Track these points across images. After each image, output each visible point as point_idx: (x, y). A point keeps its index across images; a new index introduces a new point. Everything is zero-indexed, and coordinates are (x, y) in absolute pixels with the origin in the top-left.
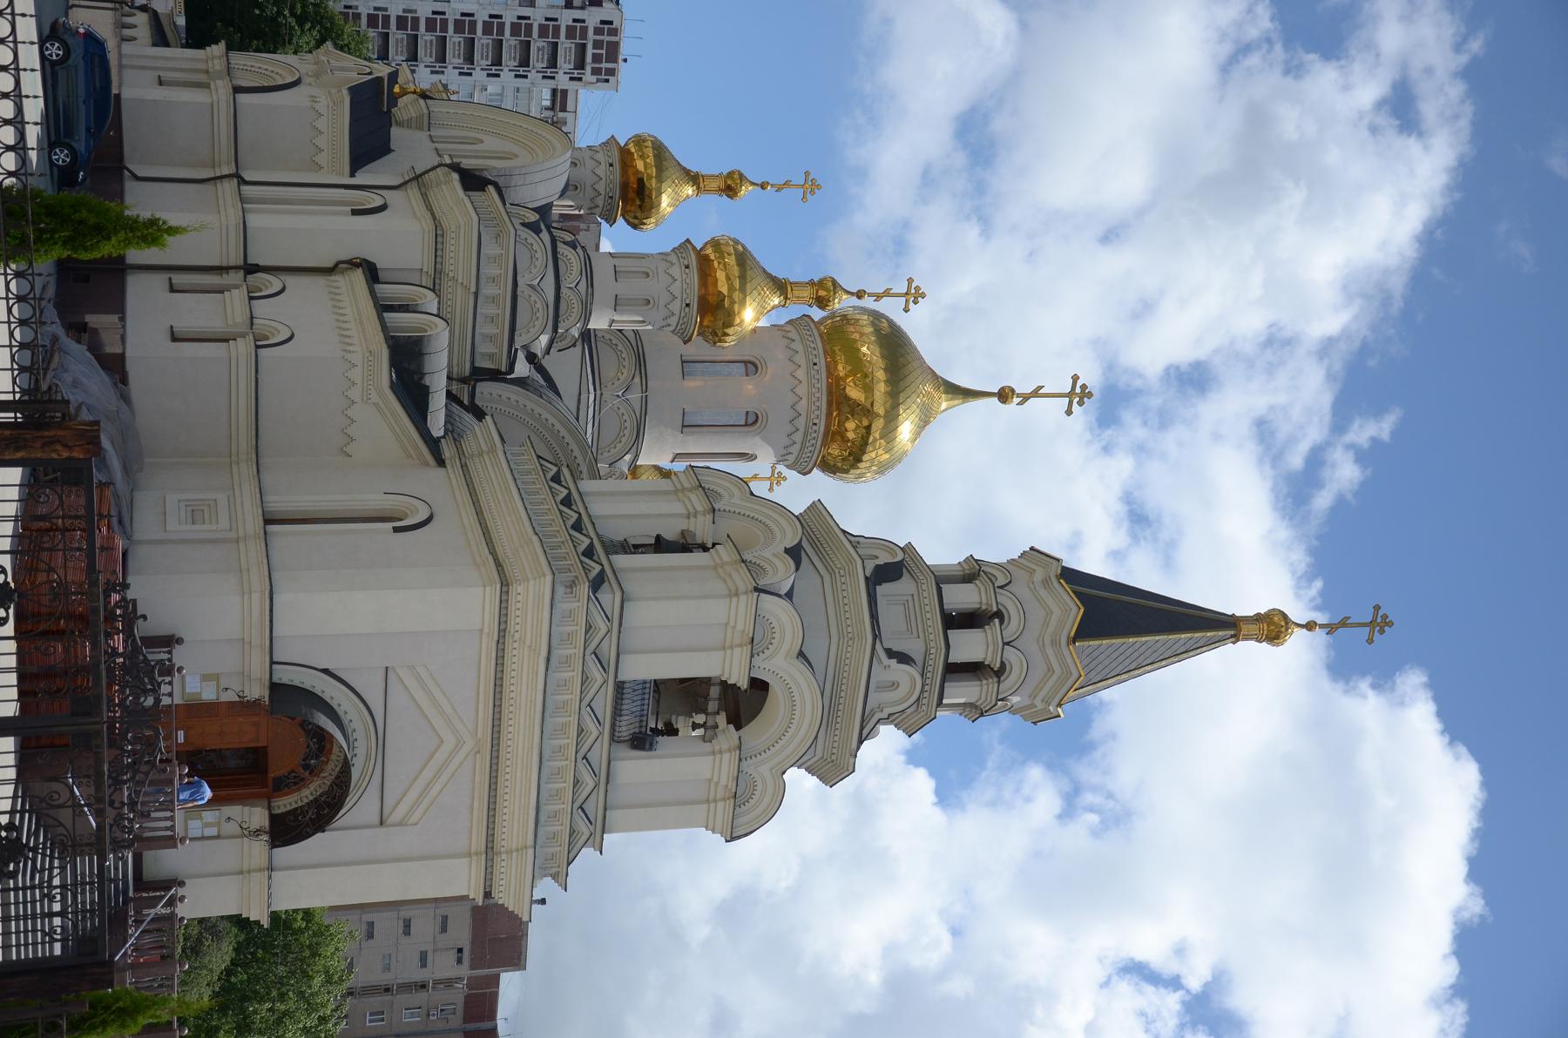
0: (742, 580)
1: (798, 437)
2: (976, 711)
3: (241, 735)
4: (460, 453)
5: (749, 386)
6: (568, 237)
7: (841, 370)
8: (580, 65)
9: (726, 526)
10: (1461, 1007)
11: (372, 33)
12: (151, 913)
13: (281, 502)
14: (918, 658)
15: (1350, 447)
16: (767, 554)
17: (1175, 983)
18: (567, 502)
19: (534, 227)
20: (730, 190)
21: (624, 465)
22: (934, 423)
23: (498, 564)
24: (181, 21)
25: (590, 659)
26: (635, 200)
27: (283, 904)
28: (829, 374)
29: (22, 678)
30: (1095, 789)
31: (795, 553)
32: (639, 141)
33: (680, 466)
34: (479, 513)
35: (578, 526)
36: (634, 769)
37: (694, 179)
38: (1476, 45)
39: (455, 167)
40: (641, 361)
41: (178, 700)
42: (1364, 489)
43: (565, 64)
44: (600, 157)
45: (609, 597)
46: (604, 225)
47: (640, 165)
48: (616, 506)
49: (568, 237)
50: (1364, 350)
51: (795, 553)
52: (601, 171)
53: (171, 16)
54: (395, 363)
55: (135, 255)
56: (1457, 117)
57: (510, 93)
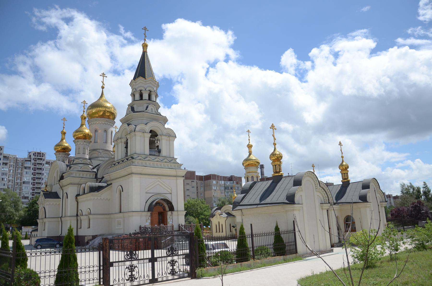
0: (133, 134)
1: (109, 123)
3: (156, 216)
4: (110, 181)
5: (99, 131)
6: (72, 162)
7: (97, 115)
8: (41, 159)
9: (123, 136)
10: (214, 27)
11: (35, 195)
12: (183, 229)
13: (118, 210)
14: (147, 105)
15: (124, 33)
16: (129, 129)
17: (208, 69)
18: (119, 163)
19: (70, 168)
20: (64, 133)
21: (113, 153)
22: (107, 100)
23: (129, 175)
24: (33, 227)
25: (145, 159)
26: (66, 150)
27: (183, 209)
28: (98, 117)
29: (146, 249)
30: (178, 79)
31: (128, 125)
32: (55, 149)
33: (113, 144)
34: (120, 178)
35: (123, 161)
36: (164, 152)
37: (62, 140)
38: (57, 7)
39: (59, 181)
41: (150, 226)
42: (132, 31)
43: (41, 162)
44: (58, 156)
45: (135, 156)
46: (70, 156)
47: (59, 149)
48: (120, 155)
49: (72, 162)
50: (108, 29)
51: (128, 125)
52: (60, 156)
53: (32, 228)
54: (94, 192)
55: (75, 233)
56: (69, 11)
57: (46, 172)
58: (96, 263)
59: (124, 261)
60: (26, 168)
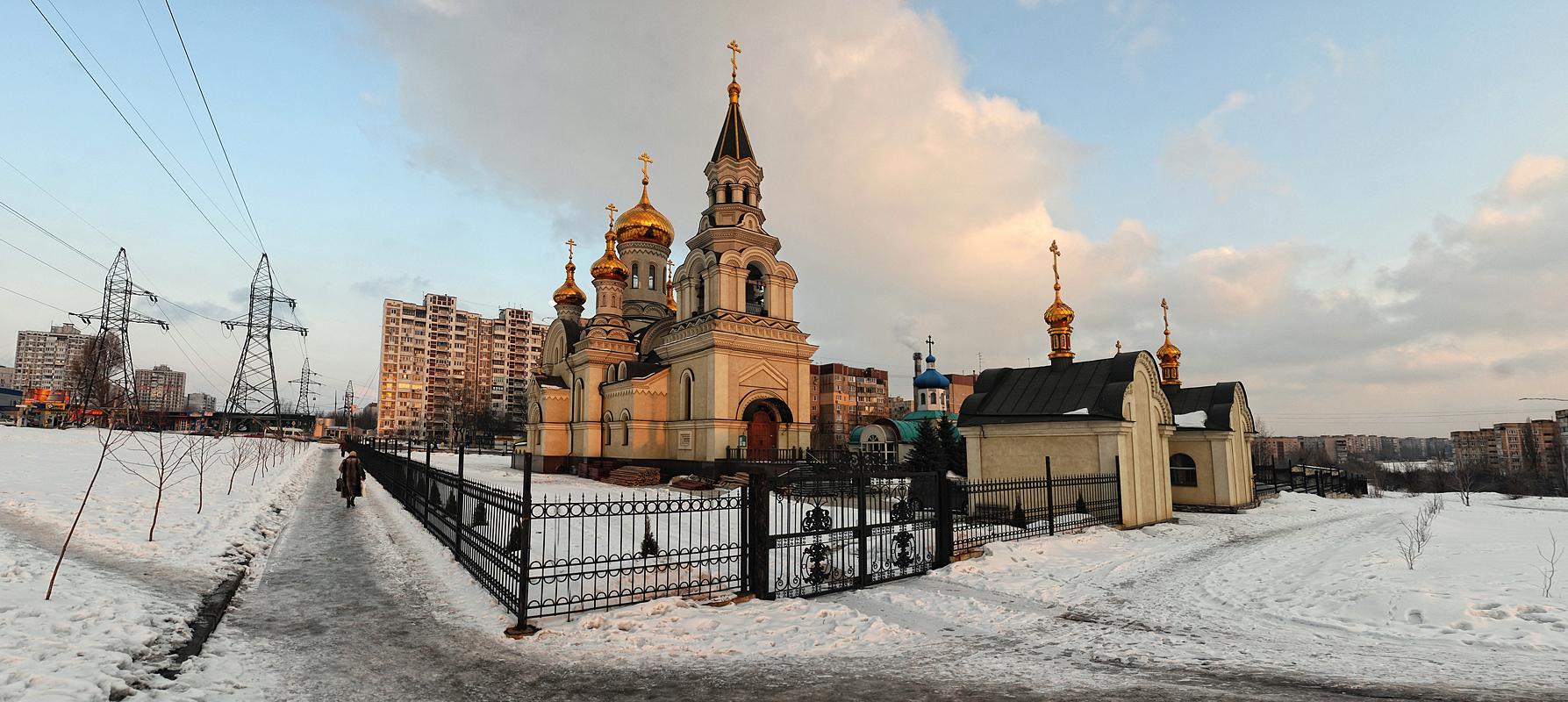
0: (714, 269)
2: (759, 197)
13: (682, 415)
20: (573, 269)
36: (775, 311)
40: (632, 302)
51: (705, 251)
58: (735, 537)
59: (801, 535)
60: (497, 336)
